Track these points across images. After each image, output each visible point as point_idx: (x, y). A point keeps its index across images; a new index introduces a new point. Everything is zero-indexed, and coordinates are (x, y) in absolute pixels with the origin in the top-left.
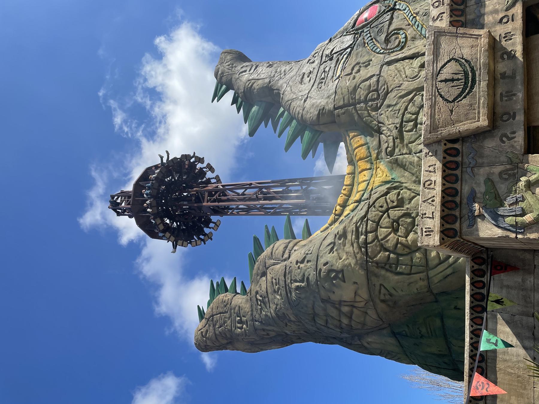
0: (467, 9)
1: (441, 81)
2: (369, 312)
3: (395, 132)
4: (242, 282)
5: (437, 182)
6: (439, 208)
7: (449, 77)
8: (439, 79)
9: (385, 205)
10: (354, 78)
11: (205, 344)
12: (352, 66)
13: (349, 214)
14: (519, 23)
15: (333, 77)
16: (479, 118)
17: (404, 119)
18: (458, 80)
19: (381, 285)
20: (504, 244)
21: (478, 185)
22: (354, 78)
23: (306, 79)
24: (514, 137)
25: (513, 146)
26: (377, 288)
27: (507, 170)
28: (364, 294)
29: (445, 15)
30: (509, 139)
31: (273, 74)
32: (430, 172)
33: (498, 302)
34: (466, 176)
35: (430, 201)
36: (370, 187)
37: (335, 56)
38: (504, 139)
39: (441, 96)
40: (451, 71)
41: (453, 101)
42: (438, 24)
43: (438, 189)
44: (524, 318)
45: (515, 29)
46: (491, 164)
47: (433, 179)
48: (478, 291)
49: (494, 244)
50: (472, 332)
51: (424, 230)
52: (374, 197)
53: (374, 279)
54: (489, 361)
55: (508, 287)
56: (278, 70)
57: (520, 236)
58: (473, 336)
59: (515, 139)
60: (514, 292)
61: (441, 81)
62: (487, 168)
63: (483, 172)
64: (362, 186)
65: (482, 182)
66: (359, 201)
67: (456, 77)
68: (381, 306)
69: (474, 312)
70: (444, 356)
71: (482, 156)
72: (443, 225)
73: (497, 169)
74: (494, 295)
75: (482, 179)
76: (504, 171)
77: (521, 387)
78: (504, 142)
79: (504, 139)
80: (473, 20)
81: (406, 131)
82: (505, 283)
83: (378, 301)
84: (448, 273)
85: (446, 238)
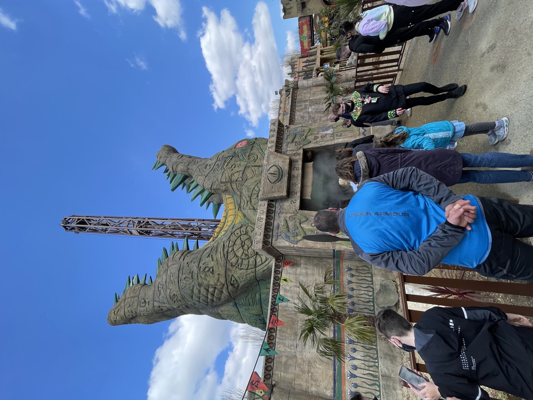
0: (282, 147)
1: (269, 173)
2: (224, 291)
3: (248, 199)
4: (151, 277)
5: (264, 218)
6: (263, 231)
7: (273, 172)
8: (269, 172)
9: (240, 233)
10: (232, 170)
11: (115, 319)
12: (232, 165)
13: (216, 212)
14: (301, 156)
15: (222, 168)
16: (283, 192)
17: (253, 193)
18: (276, 174)
19: (232, 275)
20: (289, 251)
21: (281, 221)
22: (232, 170)
23: (208, 167)
24: (296, 202)
25: (295, 206)
26: (230, 276)
27: (293, 216)
28: (222, 280)
29: (273, 147)
30: (294, 203)
31: (191, 161)
32: (261, 213)
33: (285, 280)
34: (276, 217)
35: (259, 227)
36: (233, 224)
37: (224, 158)
38: (292, 202)
39: (269, 180)
40: (273, 170)
41: (274, 183)
42: (270, 149)
43: (264, 221)
44: (295, 288)
45: (299, 159)
46: (286, 213)
47: (262, 217)
48: (276, 281)
49: (285, 251)
50: (273, 296)
51: (256, 241)
52: (234, 229)
53: (228, 272)
54: (279, 311)
55: (290, 273)
56: (194, 160)
57: (295, 246)
58: (273, 299)
59: (296, 203)
60: (292, 276)
61: (269, 173)
62: (285, 214)
63: (283, 215)
64: (229, 224)
65: (282, 220)
66: (226, 231)
67: (275, 173)
68: (230, 287)
69: (274, 286)
70: (259, 315)
71: (283, 209)
72: (264, 239)
73: (289, 215)
74: (284, 276)
75: (282, 219)
76: (291, 216)
77: (292, 324)
78: (292, 204)
79: (292, 202)
80: (284, 152)
81: (253, 199)
82: (289, 272)
83: (229, 284)
84: (265, 269)
85: (265, 245)
